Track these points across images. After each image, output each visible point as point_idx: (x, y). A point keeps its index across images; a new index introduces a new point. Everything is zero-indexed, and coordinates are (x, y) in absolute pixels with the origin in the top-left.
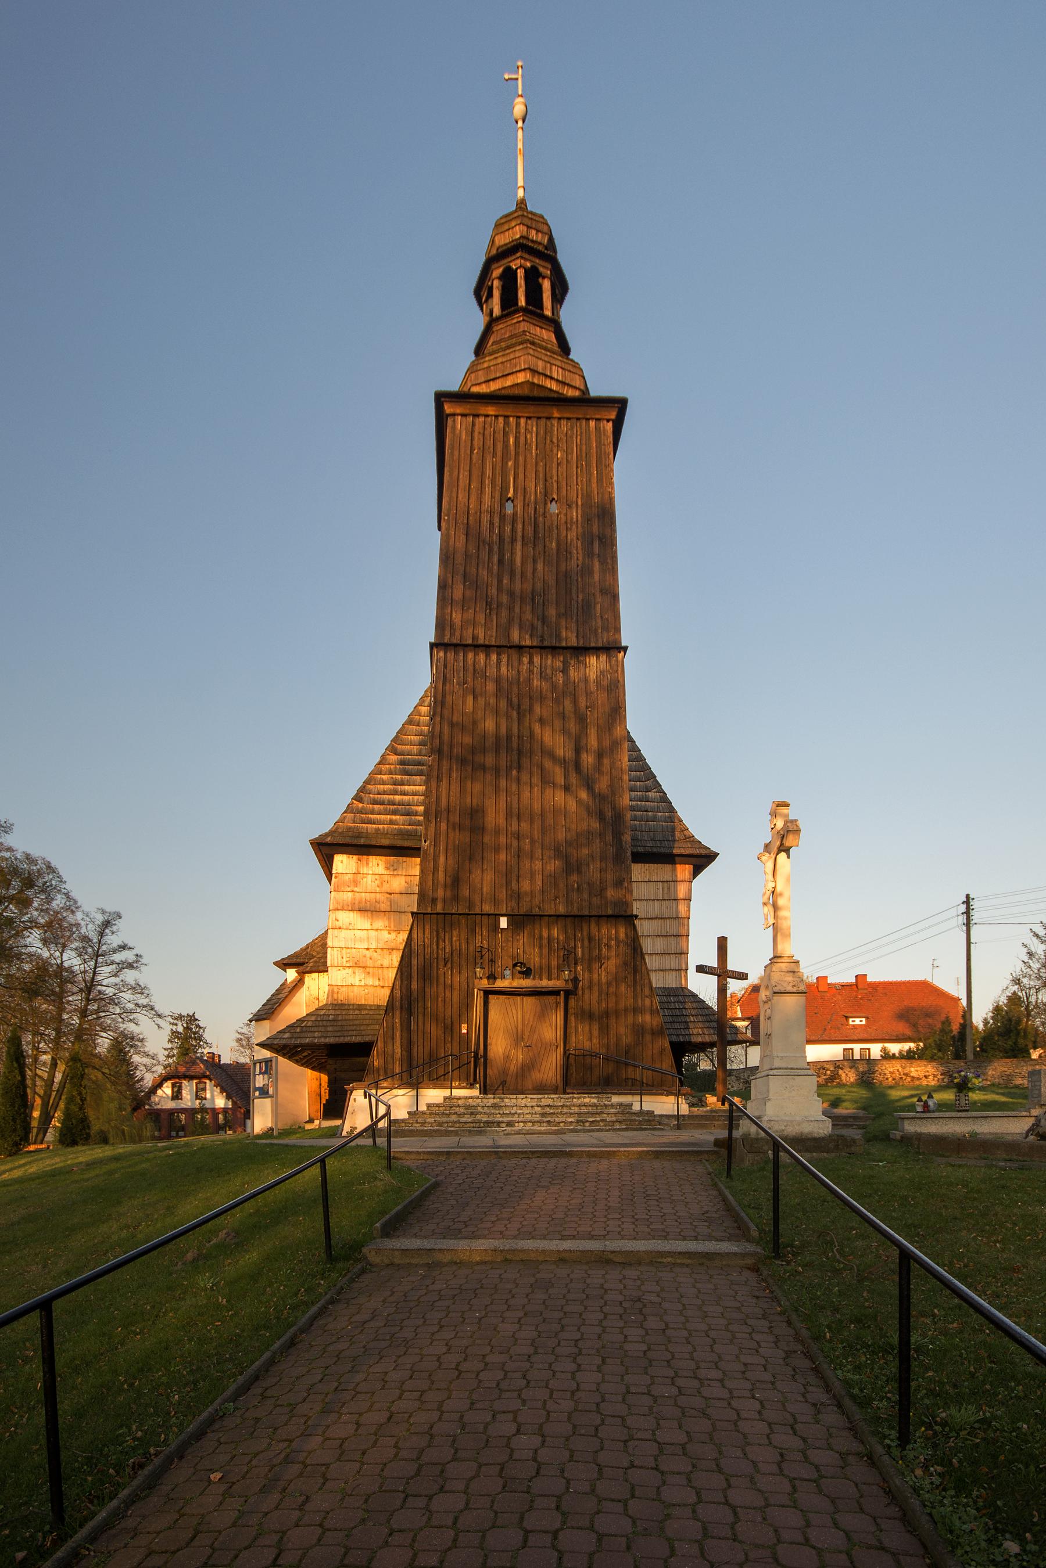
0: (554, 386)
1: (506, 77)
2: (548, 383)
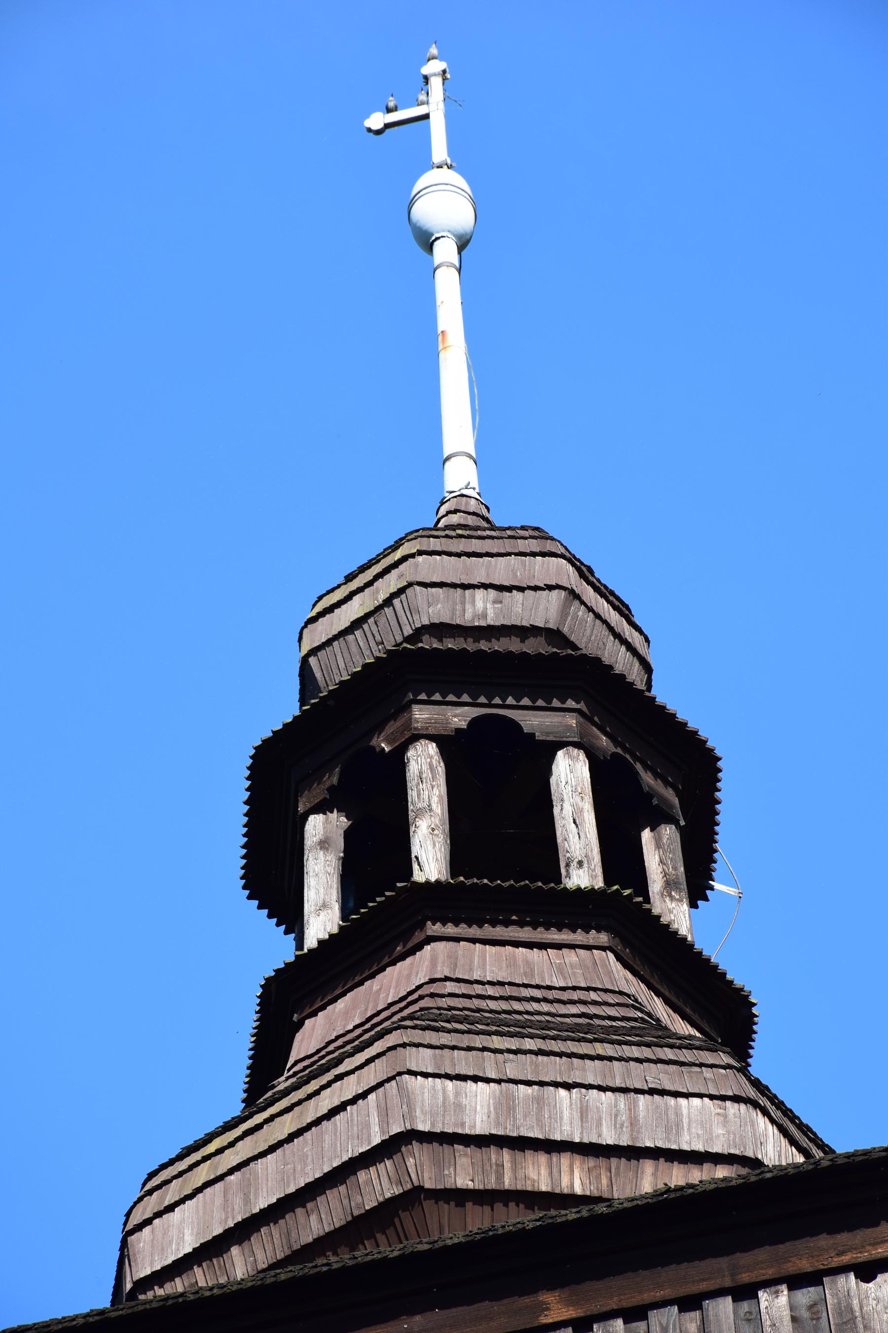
0: (576, 1178)
1: (376, 121)
2: (538, 1174)
